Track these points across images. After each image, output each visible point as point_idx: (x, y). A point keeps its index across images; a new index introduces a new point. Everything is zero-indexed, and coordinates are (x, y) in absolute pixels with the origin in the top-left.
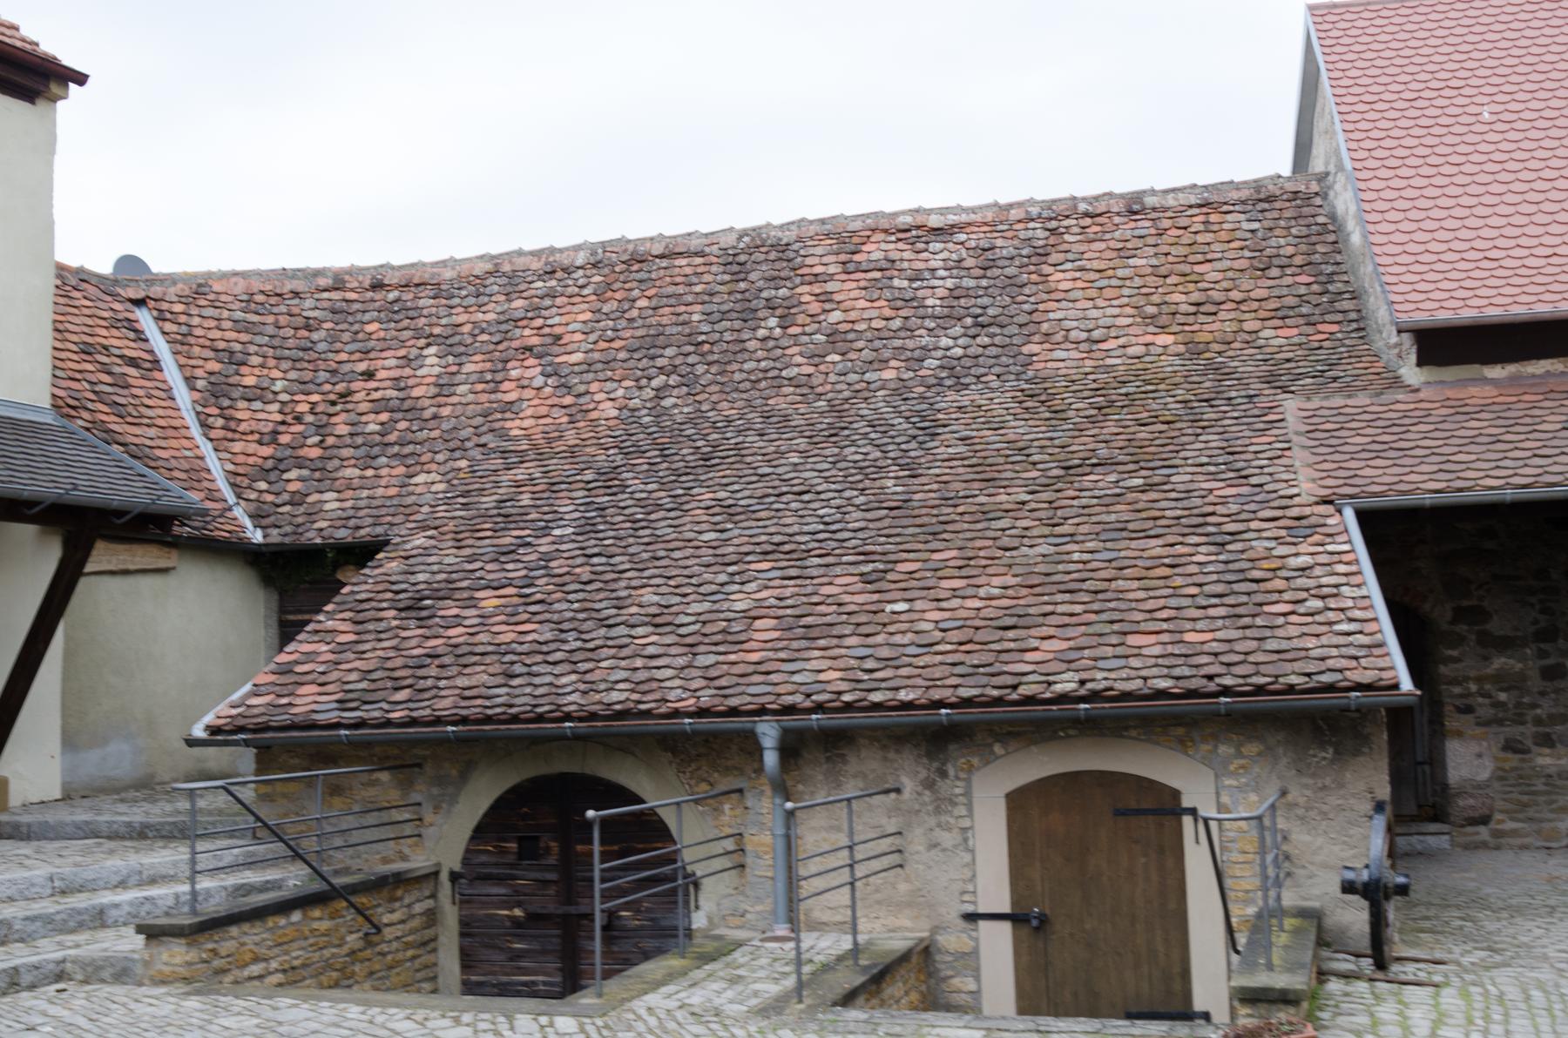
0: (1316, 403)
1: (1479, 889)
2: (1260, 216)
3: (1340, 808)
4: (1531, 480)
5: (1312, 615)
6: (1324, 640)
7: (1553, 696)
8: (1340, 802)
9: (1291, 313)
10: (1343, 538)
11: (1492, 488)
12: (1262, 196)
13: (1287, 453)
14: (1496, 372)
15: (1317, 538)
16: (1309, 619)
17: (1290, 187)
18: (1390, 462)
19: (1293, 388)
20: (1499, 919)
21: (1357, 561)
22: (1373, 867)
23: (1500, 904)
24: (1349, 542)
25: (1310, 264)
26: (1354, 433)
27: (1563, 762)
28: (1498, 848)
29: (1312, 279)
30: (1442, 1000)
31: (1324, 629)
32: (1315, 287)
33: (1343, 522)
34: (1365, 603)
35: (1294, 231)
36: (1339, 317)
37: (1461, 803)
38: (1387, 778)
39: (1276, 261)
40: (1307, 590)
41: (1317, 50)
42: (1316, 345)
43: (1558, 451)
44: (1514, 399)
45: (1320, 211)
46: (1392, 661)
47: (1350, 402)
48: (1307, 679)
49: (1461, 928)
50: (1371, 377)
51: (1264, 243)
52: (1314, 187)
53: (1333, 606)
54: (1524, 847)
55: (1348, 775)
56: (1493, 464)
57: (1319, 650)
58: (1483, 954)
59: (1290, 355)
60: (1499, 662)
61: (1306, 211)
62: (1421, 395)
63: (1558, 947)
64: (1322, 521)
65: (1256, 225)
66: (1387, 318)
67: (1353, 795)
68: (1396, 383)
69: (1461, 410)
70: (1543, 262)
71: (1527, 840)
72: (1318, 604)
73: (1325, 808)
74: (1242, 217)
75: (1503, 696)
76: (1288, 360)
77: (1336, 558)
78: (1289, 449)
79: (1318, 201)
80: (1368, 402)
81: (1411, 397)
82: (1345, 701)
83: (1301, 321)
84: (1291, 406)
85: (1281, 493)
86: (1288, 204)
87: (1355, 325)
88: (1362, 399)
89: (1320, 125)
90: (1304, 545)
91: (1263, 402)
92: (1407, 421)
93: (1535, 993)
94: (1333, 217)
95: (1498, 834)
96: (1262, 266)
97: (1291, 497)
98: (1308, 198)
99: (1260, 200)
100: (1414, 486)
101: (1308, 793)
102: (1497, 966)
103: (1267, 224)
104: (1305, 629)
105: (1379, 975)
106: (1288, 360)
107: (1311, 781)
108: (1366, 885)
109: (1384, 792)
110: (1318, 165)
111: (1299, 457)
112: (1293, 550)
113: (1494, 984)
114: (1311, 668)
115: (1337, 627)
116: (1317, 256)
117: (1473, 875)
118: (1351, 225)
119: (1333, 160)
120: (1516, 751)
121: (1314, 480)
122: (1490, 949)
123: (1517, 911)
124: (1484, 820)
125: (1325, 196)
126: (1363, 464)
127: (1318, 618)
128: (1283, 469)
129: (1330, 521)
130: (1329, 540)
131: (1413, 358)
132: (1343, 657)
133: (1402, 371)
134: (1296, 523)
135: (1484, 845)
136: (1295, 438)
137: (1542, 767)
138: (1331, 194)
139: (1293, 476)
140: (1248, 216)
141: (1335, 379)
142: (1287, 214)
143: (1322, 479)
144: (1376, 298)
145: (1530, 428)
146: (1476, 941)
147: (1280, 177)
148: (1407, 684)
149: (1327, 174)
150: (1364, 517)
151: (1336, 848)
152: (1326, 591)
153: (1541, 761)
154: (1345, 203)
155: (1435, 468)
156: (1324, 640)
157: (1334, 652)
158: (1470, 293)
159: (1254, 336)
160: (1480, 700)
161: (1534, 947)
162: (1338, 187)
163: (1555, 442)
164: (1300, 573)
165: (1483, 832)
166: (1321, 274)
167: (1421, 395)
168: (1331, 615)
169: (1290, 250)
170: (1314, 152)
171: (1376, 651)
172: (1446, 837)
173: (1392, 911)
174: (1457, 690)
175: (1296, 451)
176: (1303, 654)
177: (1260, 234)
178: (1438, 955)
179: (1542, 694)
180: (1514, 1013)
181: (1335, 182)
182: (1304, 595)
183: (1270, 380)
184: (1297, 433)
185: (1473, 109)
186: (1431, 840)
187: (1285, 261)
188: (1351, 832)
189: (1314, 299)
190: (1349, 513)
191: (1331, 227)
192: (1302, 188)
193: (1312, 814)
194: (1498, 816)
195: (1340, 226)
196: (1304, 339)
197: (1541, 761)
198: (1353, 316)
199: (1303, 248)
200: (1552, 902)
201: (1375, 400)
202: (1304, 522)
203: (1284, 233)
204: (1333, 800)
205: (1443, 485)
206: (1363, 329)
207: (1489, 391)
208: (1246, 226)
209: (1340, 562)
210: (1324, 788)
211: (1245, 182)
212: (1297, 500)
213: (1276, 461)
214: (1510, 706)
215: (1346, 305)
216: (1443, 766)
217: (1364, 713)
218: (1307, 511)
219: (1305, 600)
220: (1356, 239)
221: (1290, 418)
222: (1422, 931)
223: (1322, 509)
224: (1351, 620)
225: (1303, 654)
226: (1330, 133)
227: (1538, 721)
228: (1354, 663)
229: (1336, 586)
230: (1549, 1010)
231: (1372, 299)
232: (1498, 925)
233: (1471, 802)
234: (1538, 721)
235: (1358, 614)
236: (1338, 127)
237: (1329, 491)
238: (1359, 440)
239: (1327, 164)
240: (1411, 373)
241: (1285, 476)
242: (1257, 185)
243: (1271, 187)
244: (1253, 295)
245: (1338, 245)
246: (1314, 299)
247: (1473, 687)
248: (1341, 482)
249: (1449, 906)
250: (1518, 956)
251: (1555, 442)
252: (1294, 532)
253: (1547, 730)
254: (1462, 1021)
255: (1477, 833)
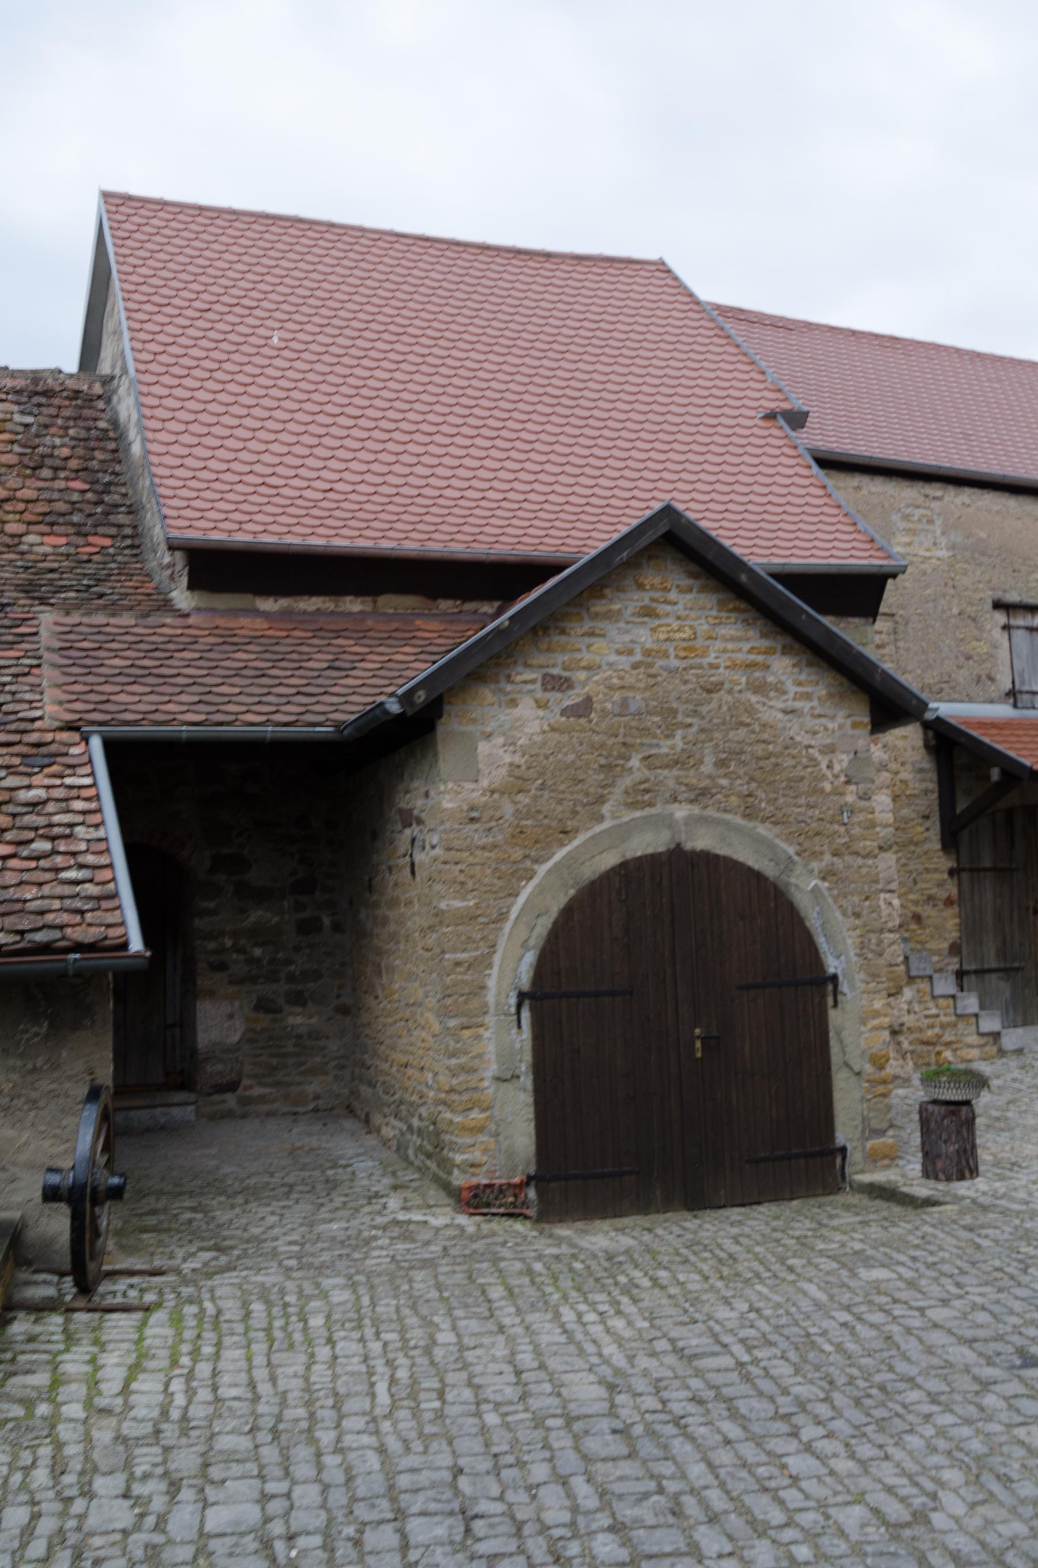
0: (75, 618)
1: (218, 1168)
2: (35, 411)
3: (53, 1095)
4: (293, 718)
5: (37, 858)
6: (46, 890)
7: (307, 951)
8: (53, 1086)
9: (61, 520)
10: (87, 770)
11: (252, 724)
12: (39, 388)
13: (35, 671)
14: (268, 604)
15: (55, 768)
16: (33, 864)
17: (70, 384)
18: (148, 689)
19: (52, 601)
20: (232, 1207)
21: (97, 797)
22: (78, 1168)
23: (237, 1186)
24: (92, 774)
25: (85, 469)
26: (113, 654)
27: (314, 1020)
28: (244, 1116)
29: (87, 487)
30: (148, 1332)
31: (49, 876)
32: (89, 496)
33: (88, 752)
34: (102, 846)
35: (71, 432)
36: (113, 531)
37: (209, 1069)
38: (111, 1056)
39: (48, 462)
40: (36, 829)
41: (111, 249)
42: (85, 557)
43: (322, 690)
44: (284, 634)
45: (103, 415)
46: (122, 915)
47: (112, 621)
48: (18, 938)
49: (190, 1221)
50: (140, 597)
51: (37, 441)
52: (98, 389)
53: (62, 849)
54: (270, 1114)
55: (64, 1054)
56: (257, 699)
57: (38, 902)
58: (207, 1255)
59: (56, 565)
60: (257, 915)
61: (86, 412)
62: (191, 621)
63: (289, 1238)
64: (64, 750)
65: (29, 420)
66: (162, 538)
67: (70, 1078)
68: (166, 606)
69: (229, 640)
70: (320, 496)
71: (276, 1106)
72: (46, 846)
73: (34, 1095)
74: (16, 408)
75: (258, 952)
76: (52, 571)
77: (74, 793)
78: (39, 666)
79: (101, 405)
80: (133, 622)
81: (179, 622)
82: (62, 965)
83: (71, 530)
84: (47, 620)
85: (21, 715)
86: (67, 403)
87: (128, 542)
88: (126, 620)
89: (109, 326)
90: (40, 776)
91: (16, 612)
92: (171, 646)
93: (257, 1307)
94: (115, 423)
95: (245, 1101)
96: (32, 464)
97: (33, 720)
98: (90, 400)
99: (37, 393)
100: (171, 717)
101: (14, 1077)
102: (222, 1270)
103: (42, 419)
104: (26, 876)
105: (81, 1303)
106: (52, 571)
107: (19, 1063)
108: (72, 1189)
109: (106, 1074)
110: (105, 368)
111: (47, 675)
112: (25, 781)
113: (213, 1299)
114: (25, 924)
115: (64, 875)
116: (94, 462)
117: (214, 1151)
118: (133, 434)
119: (119, 363)
120: (268, 1011)
121: (60, 703)
122: (217, 1248)
123: (254, 1194)
124: (232, 1087)
125: (108, 401)
126: (118, 688)
127: (43, 863)
128: (27, 688)
129: (74, 751)
130: (68, 772)
131: (185, 581)
132: (66, 911)
133: (174, 594)
134: (35, 751)
135: (229, 1115)
136: (47, 655)
137: (293, 1026)
138: (115, 399)
139: (38, 697)
140: (22, 407)
141: (101, 596)
142: (66, 413)
143: (70, 702)
144: (153, 514)
145: (297, 665)
146: (203, 1239)
147: (60, 372)
148: (136, 944)
149: (113, 378)
150: (113, 749)
151: (46, 1144)
152: (56, 830)
153: (292, 1020)
154: (128, 409)
155: (196, 699)
156: (46, 890)
157: (56, 904)
158: (247, 518)
159: (16, 540)
160: (234, 956)
161: (265, 1240)
162: (122, 391)
163: (320, 681)
164: (30, 809)
165: (231, 1100)
166: (97, 482)
167: (191, 621)
168: (59, 860)
169: (65, 452)
170: (103, 354)
171: (105, 904)
172: (193, 1107)
173: (108, 1217)
174: (212, 945)
175: (46, 670)
176: (18, 906)
177: (33, 430)
178: (158, 1263)
179: (297, 949)
180: (228, 1341)
181: (118, 386)
182: (31, 835)
183: (29, 589)
184: (49, 649)
185: (262, 331)
186: (175, 1111)
187: (58, 463)
188: (64, 1123)
189: (88, 509)
190: (96, 743)
191: (111, 434)
192: (85, 388)
193: (18, 1103)
194: (246, 1082)
195: (121, 435)
196: (72, 550)
197: (292, 1020)
198: (128, 531)
199: (80, 451)
200: (290, 1179)
201: (140, 621)
202: (44, 750)
203: (61, 432)
204: (45, 1085)
205: (202, 717)
206: (138, 547)
207: (260, 623)
208: (17, 418)
209: (78, 798)
210: (34, 1070)
211: (21, 371)
212: (38, 724)
213: (20, 679)
214: (265, 962)
215: (122, 519)
216: (193, 1028)
217: (87, 978)
218: (49, 737)
219: (32, 841)
220: (136, 449)
221: (44, 633)
222: (146, 1230)
223: (65, 736)
224: (81, 866)
225: (18, 906)
226: (117, 333)
227: (291, 978)
228: (78, 918)
229: (71, 825)
230: (268, 1330)
231: (149, 515)
232: (229, 1215)
233: (219, 1067)
234: (291, 978)
235: (90, 859)
236: (125, 324)
237: (77, 716)
238: (117, 662)
239: (113, 367)
240: (182, 598)
241: (28, 696)
242: (35, 376)
243: (50, 381)
244: (19, 494)
245: (119, 453)
246: (88, 509)
247: (229, 943)
248: (91, 707)
249: (181, 1194)
250: (245, 1254)
251: (320, 681)
252: (30, 761)
253: (300, 987)
254: (165, 1363)
255: (224, 1102)
